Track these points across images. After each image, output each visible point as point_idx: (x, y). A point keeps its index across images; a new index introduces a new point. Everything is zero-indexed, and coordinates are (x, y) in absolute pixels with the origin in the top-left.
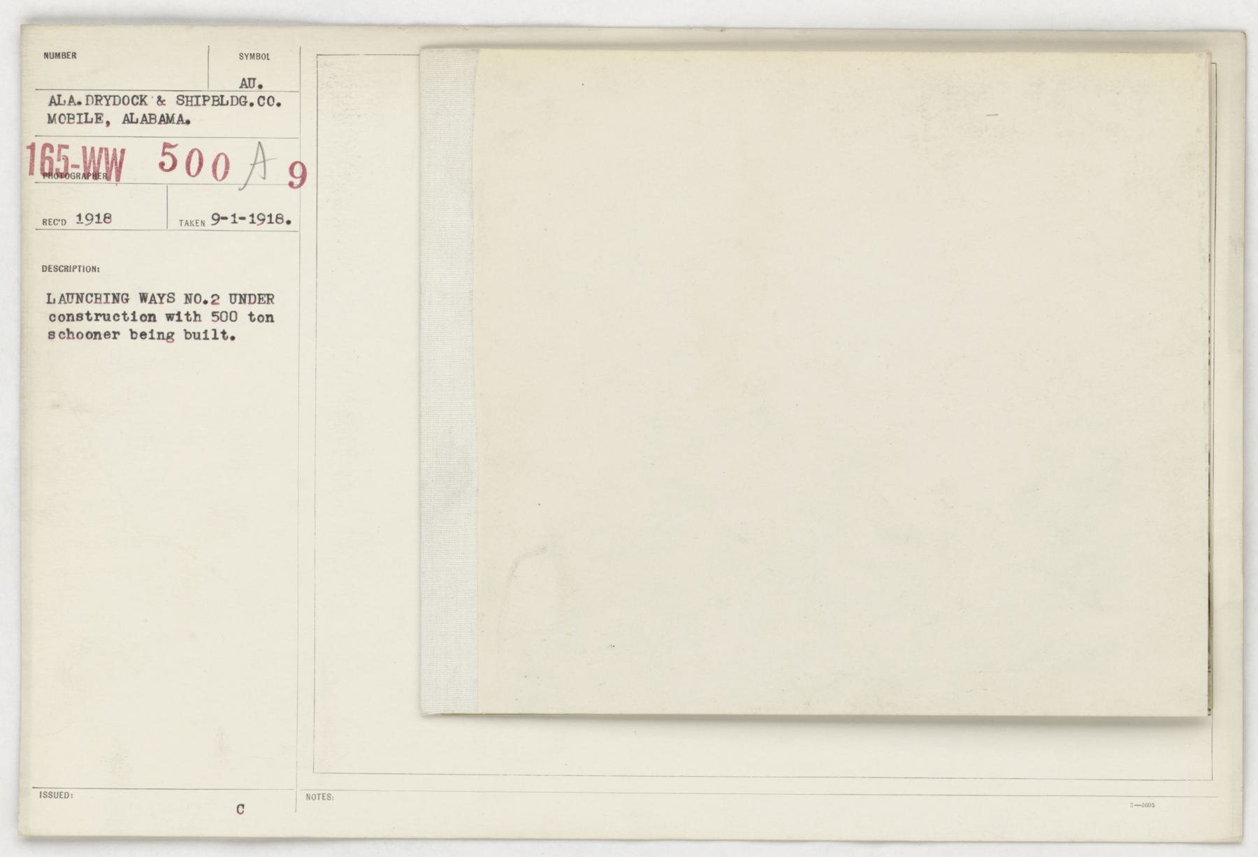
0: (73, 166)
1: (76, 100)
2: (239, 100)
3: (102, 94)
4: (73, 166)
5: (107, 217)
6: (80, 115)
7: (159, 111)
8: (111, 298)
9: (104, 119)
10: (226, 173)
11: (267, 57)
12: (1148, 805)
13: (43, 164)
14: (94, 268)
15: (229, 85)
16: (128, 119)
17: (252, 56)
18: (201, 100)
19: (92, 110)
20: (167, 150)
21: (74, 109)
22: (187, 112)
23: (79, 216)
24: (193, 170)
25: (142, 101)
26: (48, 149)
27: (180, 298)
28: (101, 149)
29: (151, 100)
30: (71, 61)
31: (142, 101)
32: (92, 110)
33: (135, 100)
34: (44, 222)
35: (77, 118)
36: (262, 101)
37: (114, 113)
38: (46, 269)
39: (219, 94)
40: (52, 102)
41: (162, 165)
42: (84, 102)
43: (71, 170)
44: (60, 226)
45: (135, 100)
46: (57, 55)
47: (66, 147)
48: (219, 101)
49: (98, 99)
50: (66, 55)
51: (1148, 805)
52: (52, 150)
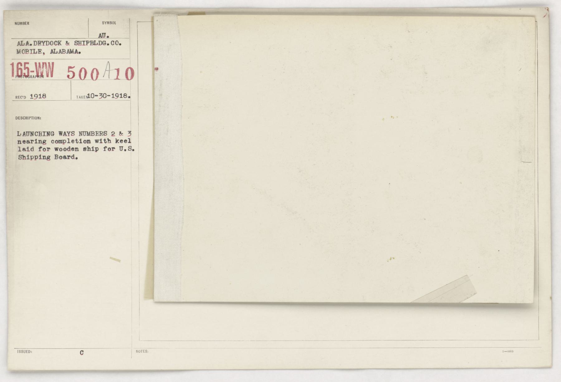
0: (31, 72)
2: (102, 43)
3: (41, 40)
4: (31, 72)
5: (44, 96)
6: (31, 50)
7: (67, 48)
8: (46, 134)
9: (42, 52)
10: (97, 77)
12: (510, 351)
13: (18, 72)
14: (39, 118)
15: (94, 37)
16: (52, 52)
17: (108, 23)
18: (85, 43)
19: (37, 48)
20: (70, 70)
21: (29, 47)
22: (79, 48)
23: (32, 95)
25: (59, 43)
26: (19, 65)
27: (77, 134)
28: (43, 63)
29: (63, 43)
31: (59, 43)
33: (56, 43)
34: (16, 97)
35: (30, 51)
36: (113, 43)
37: (46, 49)
38: (17, 118)
39: (93, 40)
40: (19, 44)
41: (68, 76)
42: (33, 44)
43: (31, 74)
44: (23, 99)
45: (56, 43)
46: (21, 23)
47: (28, 63)
48: (93, 43)
49: (39, 43)
50: (24, 23)
51: (510, 351)
52: (21, 65)
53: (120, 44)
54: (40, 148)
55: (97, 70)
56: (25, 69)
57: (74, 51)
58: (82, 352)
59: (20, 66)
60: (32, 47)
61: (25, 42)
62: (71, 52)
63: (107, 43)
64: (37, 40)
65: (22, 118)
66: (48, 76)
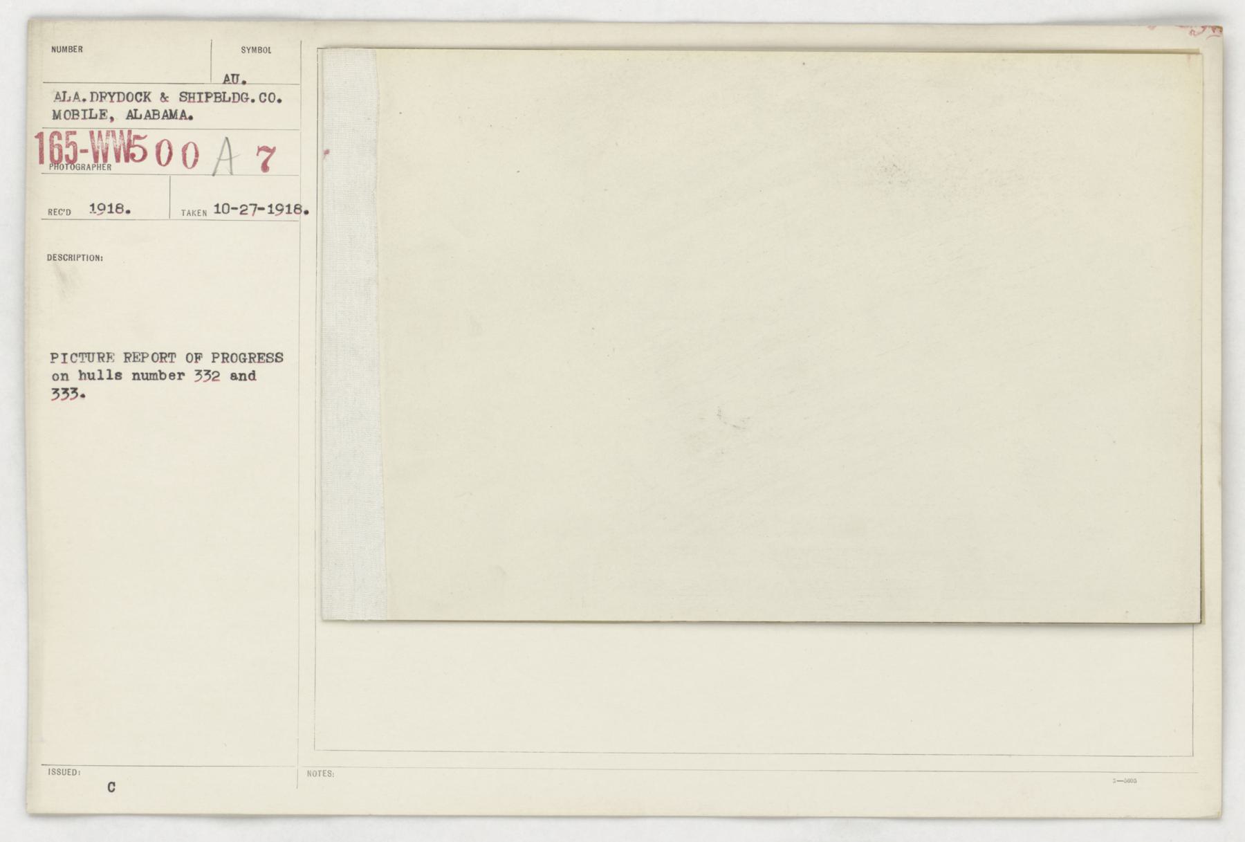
0: (82, 151)
1: (81, 98)
4: (82, 151)
7: (162, 107)
9: (108, 115)
10: (195, 162)
11: (268, 50)
12: (1129, 781)
14: (98, 257)
16: (132, 116)
17: (254, 49)
18: (203, 97)
19: (97, 106)
22: (190, 108)
24: (164, 159)
26: (56, 137)
29: (155, 97)
30: (78, 54)
31: (146, 97)
32: (97, 106)
33: (139, 97)
34: (50, 212)
36: (263, 97)
37: (118, 110)
42: (89, 98)
45: (139, 97)
46: (64, 49)
48: (220, 97)
49: (102, 96)
50: (72, 49)
51: (1129, 781)
52: (60, 138)
53: (279, 101)
56: (67, 146)
60: (87, 105)
61: (70, 94)
62: (172, 115)
63: (251, 97)
66: (118, 160)
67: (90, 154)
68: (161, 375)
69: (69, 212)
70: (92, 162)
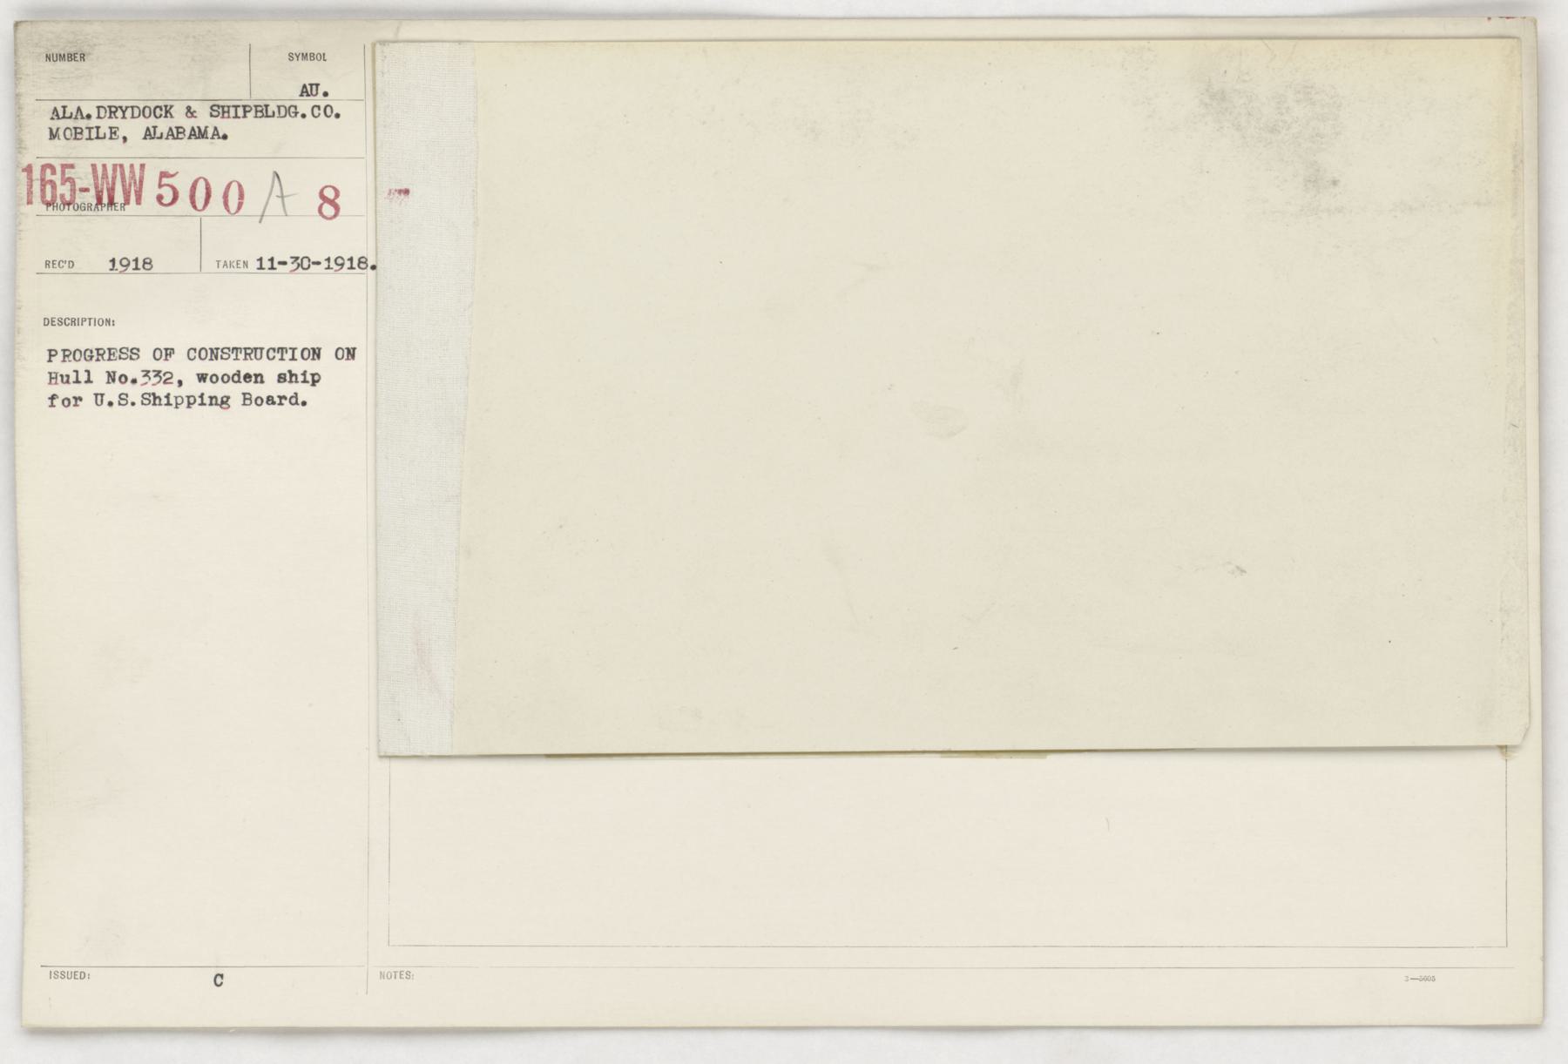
2: (288, 111)
3: (117, 104)
6: (90, 129)
7: (188, 124)
9: (121, 134)
11: (323, 57)
12: (1426, 979)
13: (43, 191)
14: (108, 321)
16: (149, 134)
17: (305, 56)
18: (240, 112)
19: (105, 124)
20: (165, 181)
23: (113, 261)
26: (48, 171)
28: (115, 166)
29: (179, 110)
31: (168, 112)
34: (47, 264)
37: (133, 128)
41: (160, 198)
42: (94, 115)
47: (72, 166)
49: (112, 111)
51: (1426, 979)
52: (54, 172)
54: (53, 398)
55: (240, 186)
56: (63, 184)
57: (210, 131)
58: (218, 980)
59: (49, 176)
60: (94, 122)
61: (72, 109)
63: (301, 111)
64: (106, 104)
65: (62, 322)
67: (93, 192)
68: (214, 354)
69: (72, 264)
70: (94, 202)
